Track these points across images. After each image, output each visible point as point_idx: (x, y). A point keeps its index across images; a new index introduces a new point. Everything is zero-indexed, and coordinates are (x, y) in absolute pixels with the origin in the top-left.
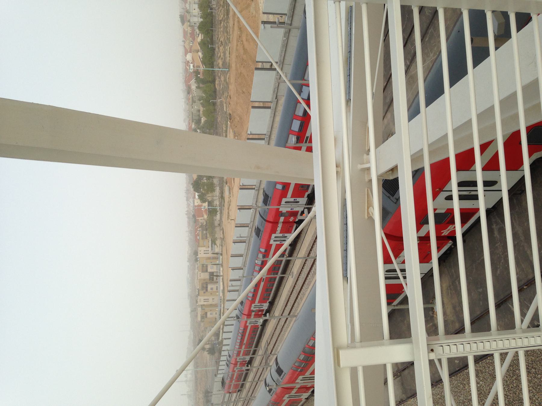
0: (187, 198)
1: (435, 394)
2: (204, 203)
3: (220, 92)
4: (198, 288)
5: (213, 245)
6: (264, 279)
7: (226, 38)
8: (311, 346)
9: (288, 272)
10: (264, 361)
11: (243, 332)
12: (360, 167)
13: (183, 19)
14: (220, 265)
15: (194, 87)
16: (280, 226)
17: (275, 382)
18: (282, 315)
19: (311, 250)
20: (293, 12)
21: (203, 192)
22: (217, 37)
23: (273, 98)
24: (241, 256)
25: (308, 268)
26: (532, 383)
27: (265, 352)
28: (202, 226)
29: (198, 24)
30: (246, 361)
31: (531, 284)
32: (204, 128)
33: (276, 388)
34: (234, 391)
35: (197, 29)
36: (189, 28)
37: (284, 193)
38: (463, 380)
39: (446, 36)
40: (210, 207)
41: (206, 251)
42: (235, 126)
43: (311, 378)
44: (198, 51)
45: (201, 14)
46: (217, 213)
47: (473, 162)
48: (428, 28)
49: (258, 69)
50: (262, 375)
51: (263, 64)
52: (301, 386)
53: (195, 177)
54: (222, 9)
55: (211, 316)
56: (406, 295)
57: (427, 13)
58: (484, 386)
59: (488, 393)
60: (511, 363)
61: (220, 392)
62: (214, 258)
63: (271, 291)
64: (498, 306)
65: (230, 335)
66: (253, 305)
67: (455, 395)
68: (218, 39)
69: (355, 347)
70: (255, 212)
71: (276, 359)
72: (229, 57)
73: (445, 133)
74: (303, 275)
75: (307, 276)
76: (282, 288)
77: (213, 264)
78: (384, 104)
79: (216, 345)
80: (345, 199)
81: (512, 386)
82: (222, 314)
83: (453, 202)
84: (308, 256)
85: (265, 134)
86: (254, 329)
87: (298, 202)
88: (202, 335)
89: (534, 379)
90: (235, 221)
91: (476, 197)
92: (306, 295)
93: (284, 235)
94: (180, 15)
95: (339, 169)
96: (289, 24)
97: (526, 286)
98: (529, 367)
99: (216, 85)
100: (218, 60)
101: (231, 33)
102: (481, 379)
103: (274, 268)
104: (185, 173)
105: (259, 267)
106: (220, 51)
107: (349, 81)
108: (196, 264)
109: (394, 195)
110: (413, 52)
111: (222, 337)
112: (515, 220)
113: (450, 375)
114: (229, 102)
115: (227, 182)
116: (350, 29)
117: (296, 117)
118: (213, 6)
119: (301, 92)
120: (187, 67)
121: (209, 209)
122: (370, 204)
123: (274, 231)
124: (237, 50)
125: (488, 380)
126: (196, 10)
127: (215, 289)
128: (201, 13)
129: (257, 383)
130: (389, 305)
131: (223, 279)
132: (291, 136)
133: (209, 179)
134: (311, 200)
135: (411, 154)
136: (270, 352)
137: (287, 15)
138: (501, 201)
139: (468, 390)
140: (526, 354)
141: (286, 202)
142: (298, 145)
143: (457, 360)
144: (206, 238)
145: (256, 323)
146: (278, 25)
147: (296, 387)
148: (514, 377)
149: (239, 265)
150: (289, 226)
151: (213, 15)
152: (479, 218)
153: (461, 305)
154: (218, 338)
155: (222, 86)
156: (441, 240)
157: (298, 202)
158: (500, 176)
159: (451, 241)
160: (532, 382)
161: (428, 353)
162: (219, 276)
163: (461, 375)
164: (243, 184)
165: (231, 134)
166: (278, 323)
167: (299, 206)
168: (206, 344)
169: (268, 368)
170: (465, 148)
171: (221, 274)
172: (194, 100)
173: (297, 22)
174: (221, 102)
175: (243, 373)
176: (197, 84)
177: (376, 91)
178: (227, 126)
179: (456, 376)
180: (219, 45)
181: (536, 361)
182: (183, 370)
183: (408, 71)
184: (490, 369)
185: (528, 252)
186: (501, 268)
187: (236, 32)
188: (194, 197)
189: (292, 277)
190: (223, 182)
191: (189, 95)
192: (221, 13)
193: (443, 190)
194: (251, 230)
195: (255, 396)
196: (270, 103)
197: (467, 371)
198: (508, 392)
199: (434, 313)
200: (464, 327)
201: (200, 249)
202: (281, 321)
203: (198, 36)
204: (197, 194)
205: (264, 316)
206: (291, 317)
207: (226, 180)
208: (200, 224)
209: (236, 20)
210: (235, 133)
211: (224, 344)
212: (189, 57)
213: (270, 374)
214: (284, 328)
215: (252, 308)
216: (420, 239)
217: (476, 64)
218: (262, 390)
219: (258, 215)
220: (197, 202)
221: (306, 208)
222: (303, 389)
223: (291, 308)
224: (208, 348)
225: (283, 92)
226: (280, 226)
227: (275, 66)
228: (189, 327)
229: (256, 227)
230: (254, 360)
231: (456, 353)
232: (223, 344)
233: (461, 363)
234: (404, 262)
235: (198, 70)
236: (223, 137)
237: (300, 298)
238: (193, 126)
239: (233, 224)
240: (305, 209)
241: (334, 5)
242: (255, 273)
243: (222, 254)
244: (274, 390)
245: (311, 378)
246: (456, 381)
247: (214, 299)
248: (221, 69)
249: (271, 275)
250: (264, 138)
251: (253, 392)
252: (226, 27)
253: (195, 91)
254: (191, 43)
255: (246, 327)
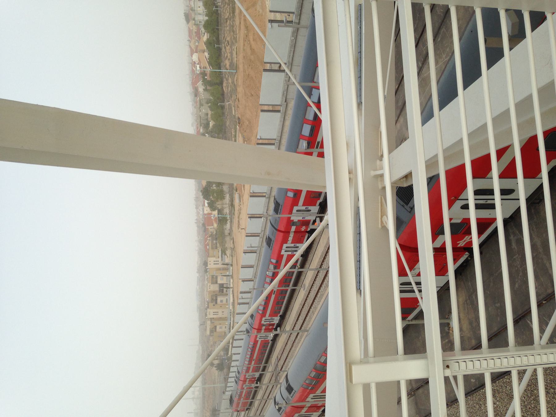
0: (196, 206)
1: (450, 415)
2: (213, 211)
3: (228, 94)
4: (208, 300)
5: (223, 255)
6: (275, 291)
7: (232, 37)
8: (322, 362)
9: (300, 284)
10: (274, 378)
11: (253, 347)
12: (373, 173)
13: (188, 18)
14: (231, 276)
15: (201, 89)
16: (292, 235)
17: (284, 400)
18: (293, 330)
19: (323, 261)
20: (301, 10)
21: (213, 199)
22: (224, 36)
23: (282, 101)
24: (251, 267)
25: (320, 281)
26: (550, 404)
27: (276, 368)
28: (211, 236)
29: (204, 23)
30: (255, 378)
31: (550, 299)
32: (213, 133)
33: (286, 407)
34: (242, 409)
35: (203, 28)
36: (194, 27)
37: (295, 201)
38: (480, 400)
39: (459, 36)
40: (220, 216)
41: (216, 261)
42: (244, 130)
43: (322, 397)
44: (204, 51)
45: (206, 12)
46: (227, 222)
47: (490, 169)
48: (439, 28)
49: (270, 71)
50: (271, 393)
51: (271, 65)
52: (311, 405)
53: (204, 183)
54: (227, 7)
55: (221, 330)
56: (422, 309)
57: (439, 11)
58: (500, 406)
59: (505, 414)
60: (529, 382)
61: (227, 410)
62: (224, 269)
63: (282, 304)
64: (516, 322)
65: (240, 350)
66: (264, 319)
67: (470, 415)
68: (224, 38)
69: (367, 363)
70: (266, 221)
71: (287, 376)
72: (237, 57)
73: (460, 138)
74: (315, 288)
75: (319, 289)
76: (293, 300)
77: (223, 276)
78: (397, 107)
79: (225, 360)
80: (358, 208)
81: (530, 407)
82: (231, 328)
83: (469, 211)
84: (320, 267)
85: (275, 139)
86: (265, 343)
87: (310, 211)
88: (211, 349)
89: (553, 399)
90: (245, 230)
91: (493, 207)
92: (319, 308)
93: (296, 245)
94: (184, 13)
95: (352, 176)
96: (296, 23)
97: (545, 301)
98: (547, 387)
99: (224, 87)
100: (225, 60)
101: (237, 32)
102: (498, 399)
103: (285, 280)
104: (194, 179)
105: (270, 279)
106: (226, 51)
107: (360, 83)
108: (205, 275)
109: (408, 203)
110: (424, 52)
111: (231, 352)
112: (533, 230)
113: (466, 395)
114: (238, 105)
115: (237, 189)
116: (360, 28)
117: (306, 121)
118: (218, 3)
119: (311, 95)
120: (193, 68)
121: (219, 217)
122: (384, 213)
123: (285, 241)
124: (244, 50)
125: (505, 401)
126: (200, 8)
127: (224, 302)
128: (206, 11)
129: (267, 400)
130: (404, 320)
131: (233, 291)
132: (301, 141)
133: (218, 186)
134: (323, 208)
135: (426, 160)
136: (280, 368)
137: (294, 14)
138: (518, 210)
139: (484, 410)
140: (545, 373)
141: (297, 211)
142: (310, 150)
143: (473, 379)
144: (216, 248)
145: (267, 337)
146: (286, 24)
147: (306, 406)
148: (532, 398)
149: (250, 277)
150: (300, 236)
151: (219, 13)
152: (496, 228)
153: (478, 320)
154: (228, 354)
155: (229, 88)
156: (457, 251)
157: (310, 211)
158: (518, 183)
159: (467, 253)
160: (550, 402)
161: (444, 369)
162: (229, 288)
163: (476, 396)
164: (253, 191)
165: (240, 139)
166: (289, 338)
167: (311, 215)
168: (214, 359)
169: (278, 385)
170: (481, 153)
171: (231, 286)
172: (202, 104)
173: (305, 20)
174: (230, 105)
175: (252, 391)
176: (204, 86)
177: (387, 94)
178: (236, 131)
179: (472, 396)
180: (226, 45)
181: (554, 381)
182: (190, 386)
183: (420, 73)
184: (507, 389)
185: (548, 265)
186: (519, 282)
187: (243, 31)
188: (204, 205)
189: (304, 290)
190: (233, 189)
191: (196, 98)
192: (227, 11)
193: (459, 198)
194: (261, 239)
195: (264, 415)
196: (279, 107)
197: (483, 391)
198: (525, 414)
199: (450, 329)
200: (481, 344)
201: (209, 259)
202: (292, 336)
203: (203, 35)
204: (206, 201)
205: (275, 331)
206: (302, 332)
207: (236, 187)
208: (210, 234)
209: (243, 18)
210: (244, 138)
211: (233, 359)
212: (195, 57)
213: (280, 392)
214: (295, 343)
215: (263, 322)
216: (436, 250)
217: (490, 65)
218: (271, 408)
219: (269, 224)
220: (207, 210)
221: (318, 217)
222: (313, 408)
223: (302, 322)
224: (217, 363)
225: (292, 95)
226: (292, 235)
227: (284, 67)
228: (197, 341)
229: (267, 237)
230: (263, 377)
231: (479, 369)
232: (232, 359)
233: (477, 382)
234: (419, 275)
235: (205, 71)
236: (232, 141)
237: (312, 311)
238: (201, 130)
239: (244, 233)
240: (317, 218)
241: (343, 2)
242: (266, 285)
243: (232, 265)
244: (284, 409)
245: (322, 397)
246: (472, 401)
247: (223, 312)
248: (228, 71)
249: (283, 287)
250: (274, 143)
251: (262, 411)
252: (232, 26)
253: (203, 94)
254: (197, 43)
255: (256, 342)
